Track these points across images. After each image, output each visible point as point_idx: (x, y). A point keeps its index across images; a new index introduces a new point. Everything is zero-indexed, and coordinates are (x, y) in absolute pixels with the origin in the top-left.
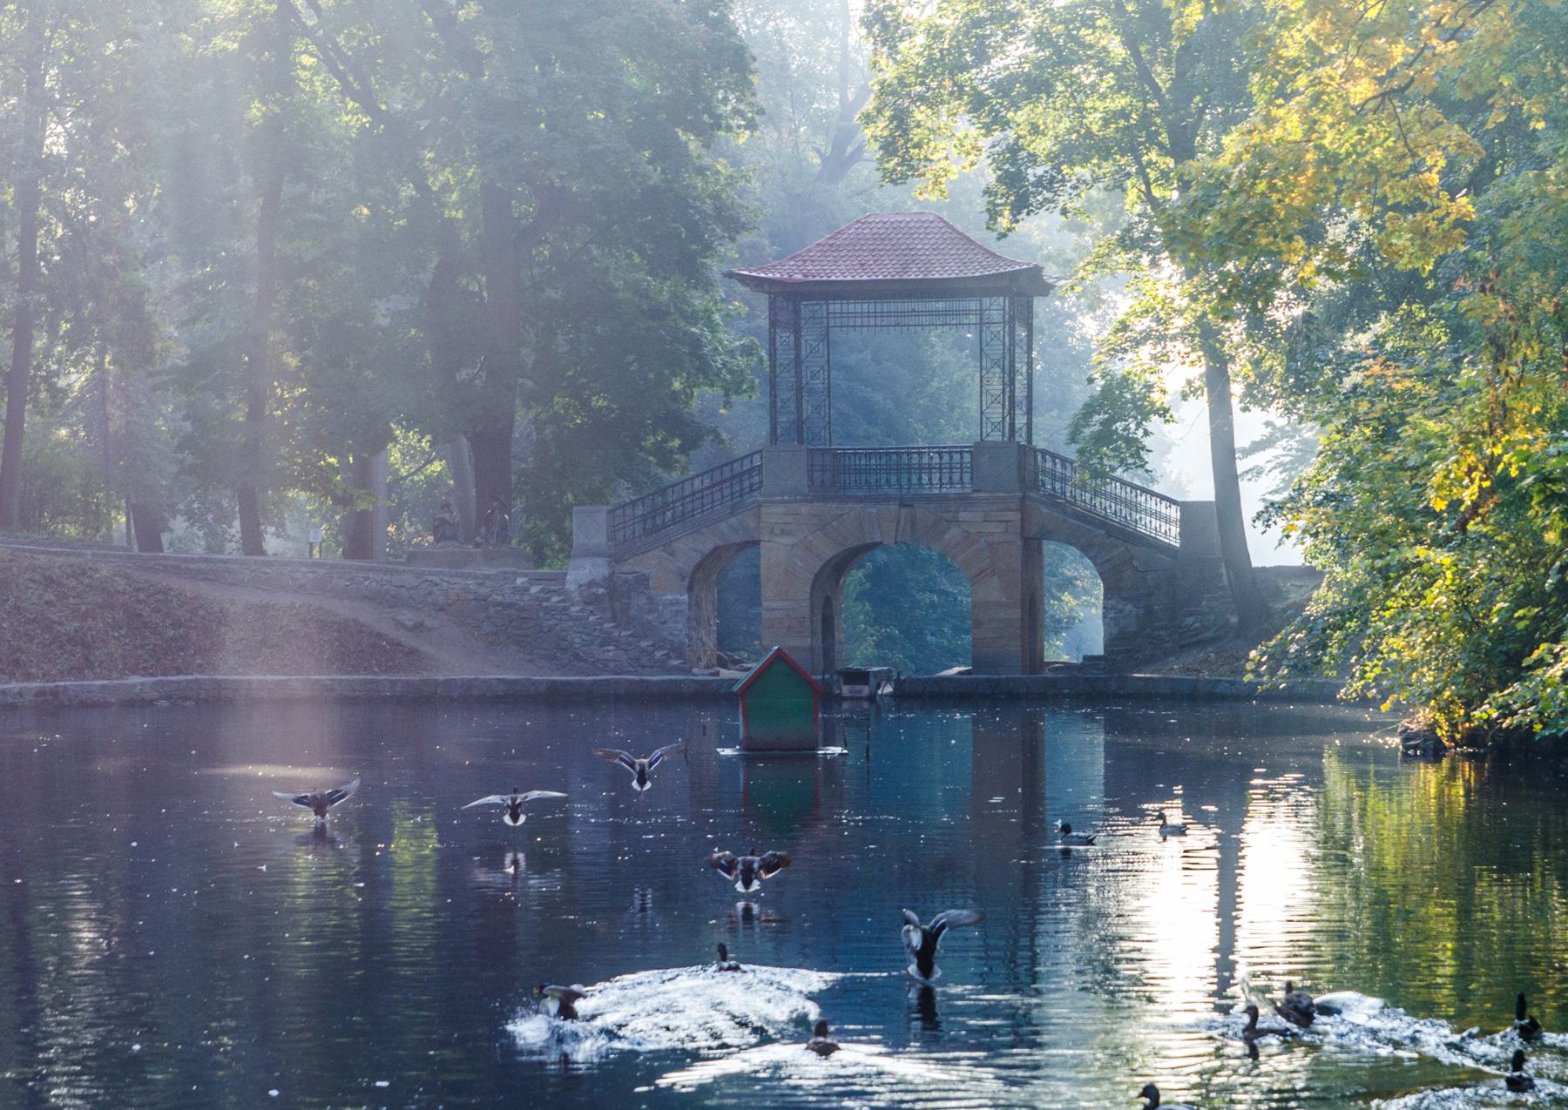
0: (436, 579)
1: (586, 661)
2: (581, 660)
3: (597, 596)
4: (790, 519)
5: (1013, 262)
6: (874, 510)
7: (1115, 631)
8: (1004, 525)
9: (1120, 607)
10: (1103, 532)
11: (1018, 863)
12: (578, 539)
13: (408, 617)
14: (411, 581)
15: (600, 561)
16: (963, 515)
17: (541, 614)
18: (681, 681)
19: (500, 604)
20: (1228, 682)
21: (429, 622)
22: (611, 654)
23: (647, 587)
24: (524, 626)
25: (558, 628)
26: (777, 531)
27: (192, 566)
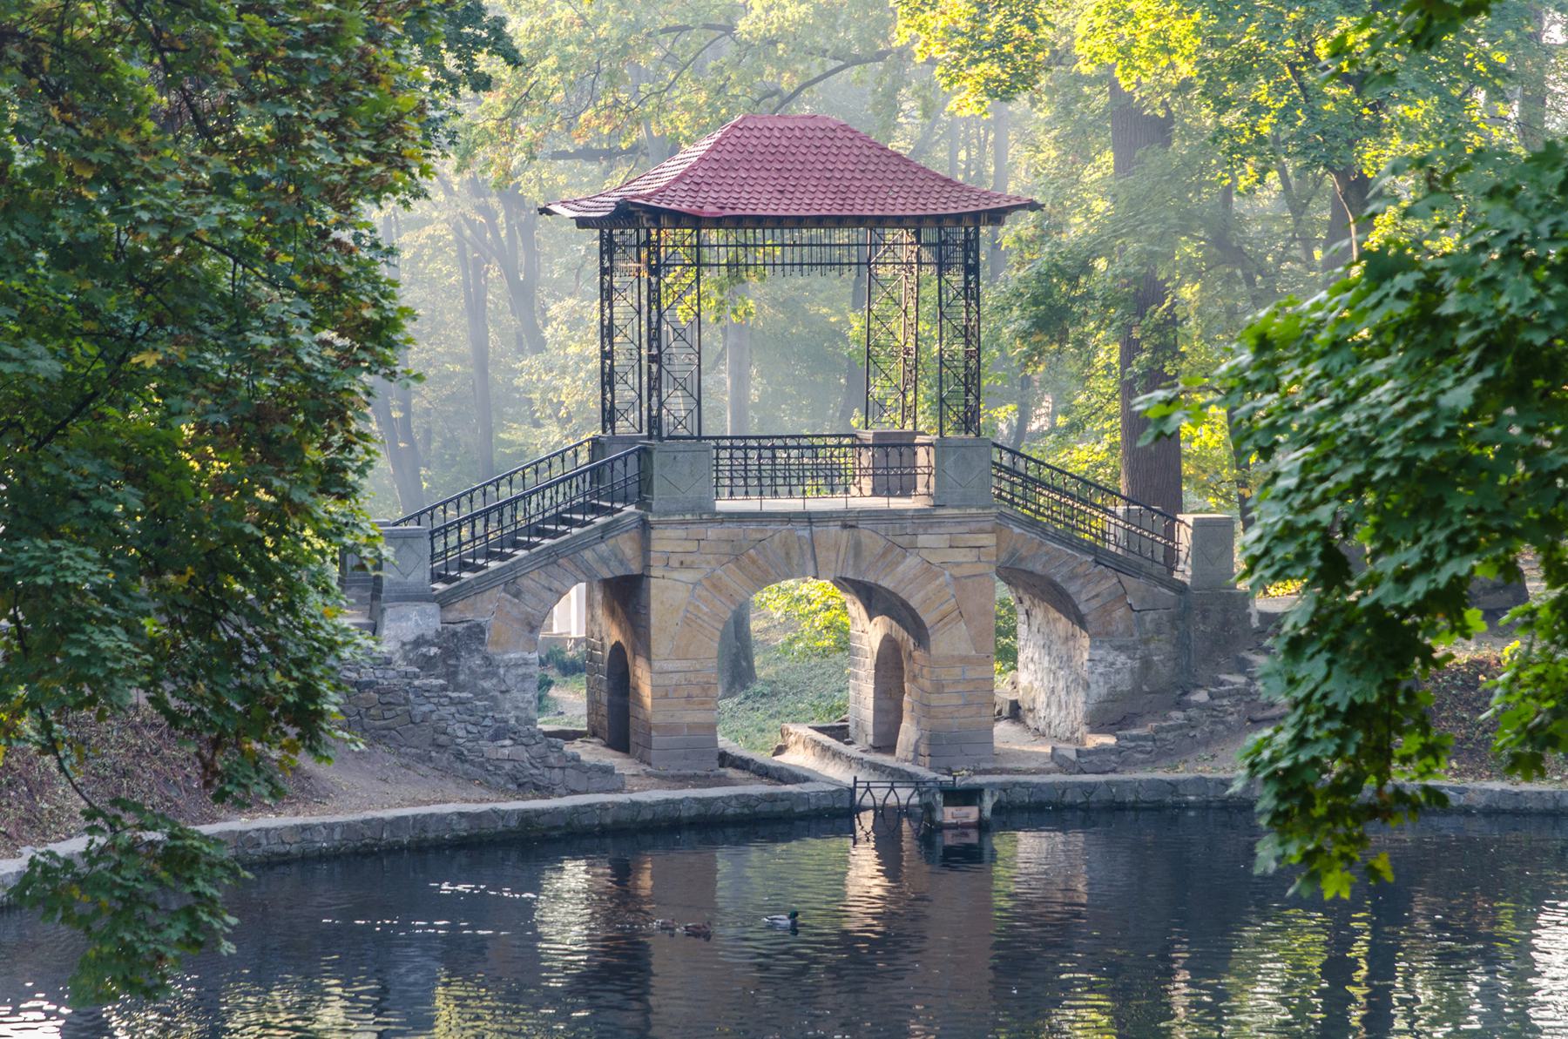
1: (472, 763)
2: (464, 761)
4: (692, 546)
8: (975, 551)
9: (1110, 659)
10: (1090, 559)
11: (498, 929)
16: (923, 540)
17: (411, 697)
22: (506, 751)
23: (482, 642)
24: (387, 714)
25: (434, 717)
26: (674, 562)
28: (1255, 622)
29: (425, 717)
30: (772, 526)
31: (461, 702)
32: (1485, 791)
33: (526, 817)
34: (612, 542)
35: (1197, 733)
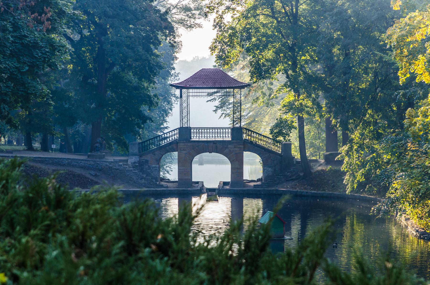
0: (99, 163)
2: (135, 183)
3: (136, 166)
4: (185, 147)
5: (242, 83)
6: (207, 145)
7: (266, 175)
9: (268, 169)
10: (263, 150)
12: (131, 150)
13: (93, 172)
14: (92, 163)
15: (137, 157)
18: (165, 190)
19: (115, 169)
20: (305, 192)
21: (98, 174)
23: (148, 163)
27: (36, 159)
28: (295, 163)
29: (128, 175)
30: (200, 143)
31: (135, 173)
32: (311, 193)
33: (134, 192)
34: (172, 146)
35: (276, 182)
